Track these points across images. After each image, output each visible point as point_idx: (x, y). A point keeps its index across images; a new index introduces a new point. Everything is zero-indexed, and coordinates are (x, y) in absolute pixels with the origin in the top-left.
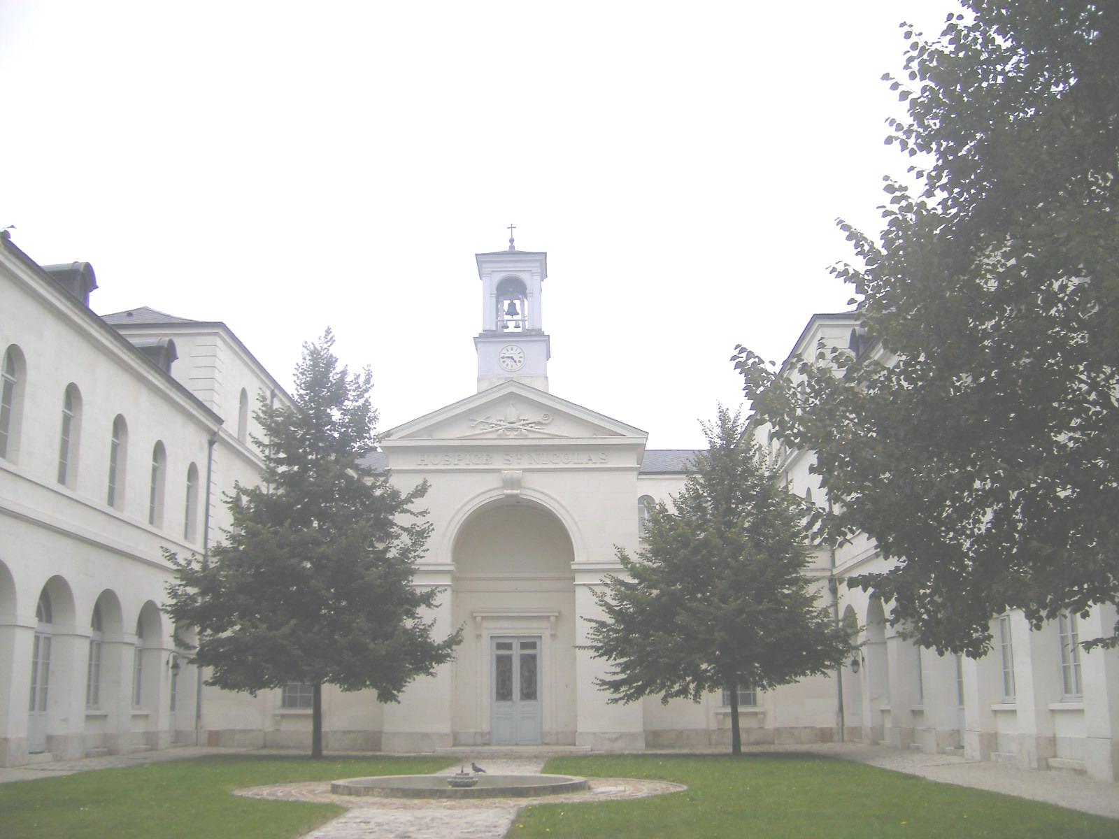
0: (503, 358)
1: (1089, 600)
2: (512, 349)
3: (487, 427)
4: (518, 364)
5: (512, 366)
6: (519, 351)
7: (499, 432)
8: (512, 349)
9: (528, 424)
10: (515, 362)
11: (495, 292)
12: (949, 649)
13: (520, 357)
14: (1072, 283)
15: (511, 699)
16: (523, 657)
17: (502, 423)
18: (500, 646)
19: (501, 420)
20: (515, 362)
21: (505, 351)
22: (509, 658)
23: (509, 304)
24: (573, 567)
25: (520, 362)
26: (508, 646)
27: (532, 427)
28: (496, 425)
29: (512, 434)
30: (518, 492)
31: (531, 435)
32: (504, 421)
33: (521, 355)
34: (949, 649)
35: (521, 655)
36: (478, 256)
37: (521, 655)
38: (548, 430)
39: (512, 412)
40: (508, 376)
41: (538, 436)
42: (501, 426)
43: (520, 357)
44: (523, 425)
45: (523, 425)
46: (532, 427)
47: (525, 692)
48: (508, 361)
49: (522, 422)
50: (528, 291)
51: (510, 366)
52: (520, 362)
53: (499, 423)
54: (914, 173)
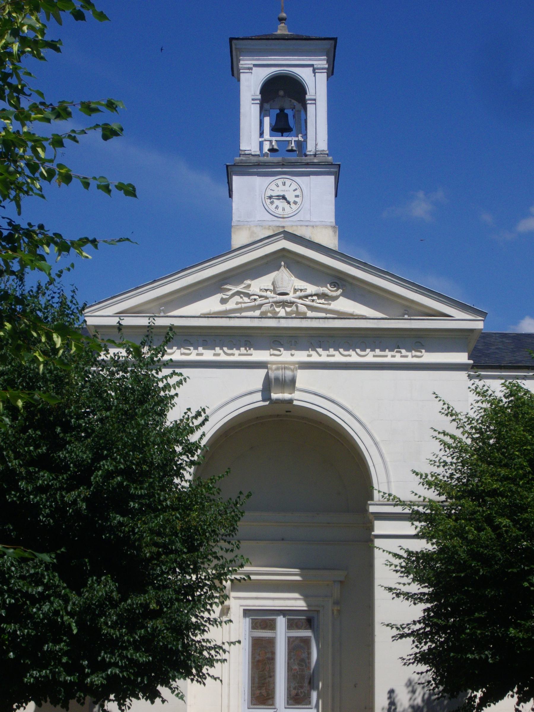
0: (270, 197)
1: (112, 694)
2: (284, 184)
3: (246, 299)
4: (293, 205)
5: (284, 209)
6: (294, 186)
7: (263, 309)
8: (284, 184)
9: (307, 297)
10: (289, 203)
11: (259, 97)
12: (48, 699)
13: (297, 196)
14: (129, 701)
15: (273, 704)
16: (290, 641)
17: (269, 294)
18: (255, 625)
19: (266, 290)
20: (289, 203)
21: (273, 186)
22: (271, 642)
23: (277, 115)
24: (372, 509)
25: (295, 203)
26: (271, 625)
27: (313, 301)
28: (260, 297)
29: (282, 312)
30: (287, 396)
31: (310, 314)
32: (271, 291)
33: (298, 193)
34: (48, 699)
35: (289, 638)
36: (234, 42)
37: (289, 638)
38: (335, 305)
39: (286, 280)
40: (278, 224)
41: (323, 315)
42: (266, 298)
43: (297, 196)
44: (300, 298)
45: (300, 298)
46: (313, 301)
47: (294, 692)
48: (277, 202)
49: (299, 294)
50: (307, 97)
51: (280, 209)
52: (295, 203)
53: (264, 294)
54: (435, 396)
